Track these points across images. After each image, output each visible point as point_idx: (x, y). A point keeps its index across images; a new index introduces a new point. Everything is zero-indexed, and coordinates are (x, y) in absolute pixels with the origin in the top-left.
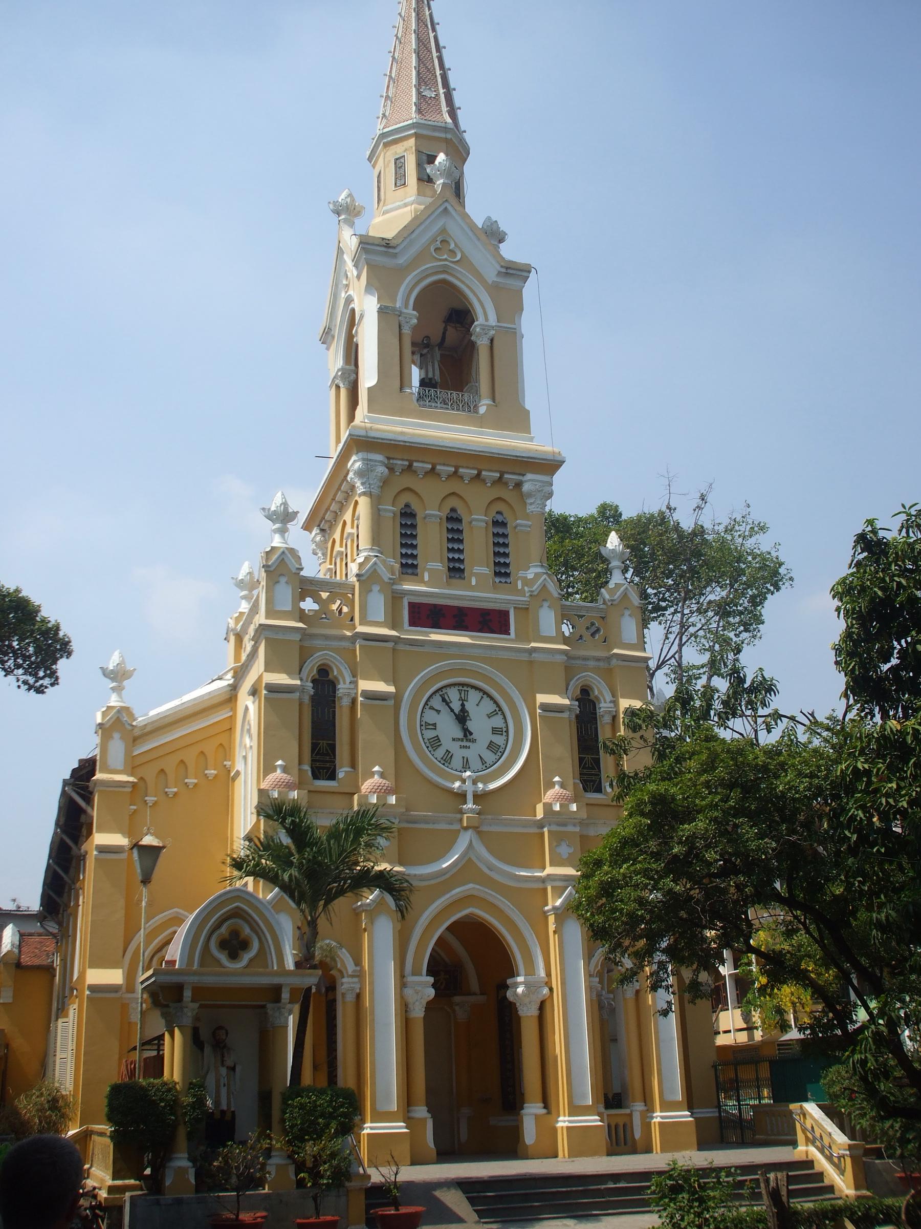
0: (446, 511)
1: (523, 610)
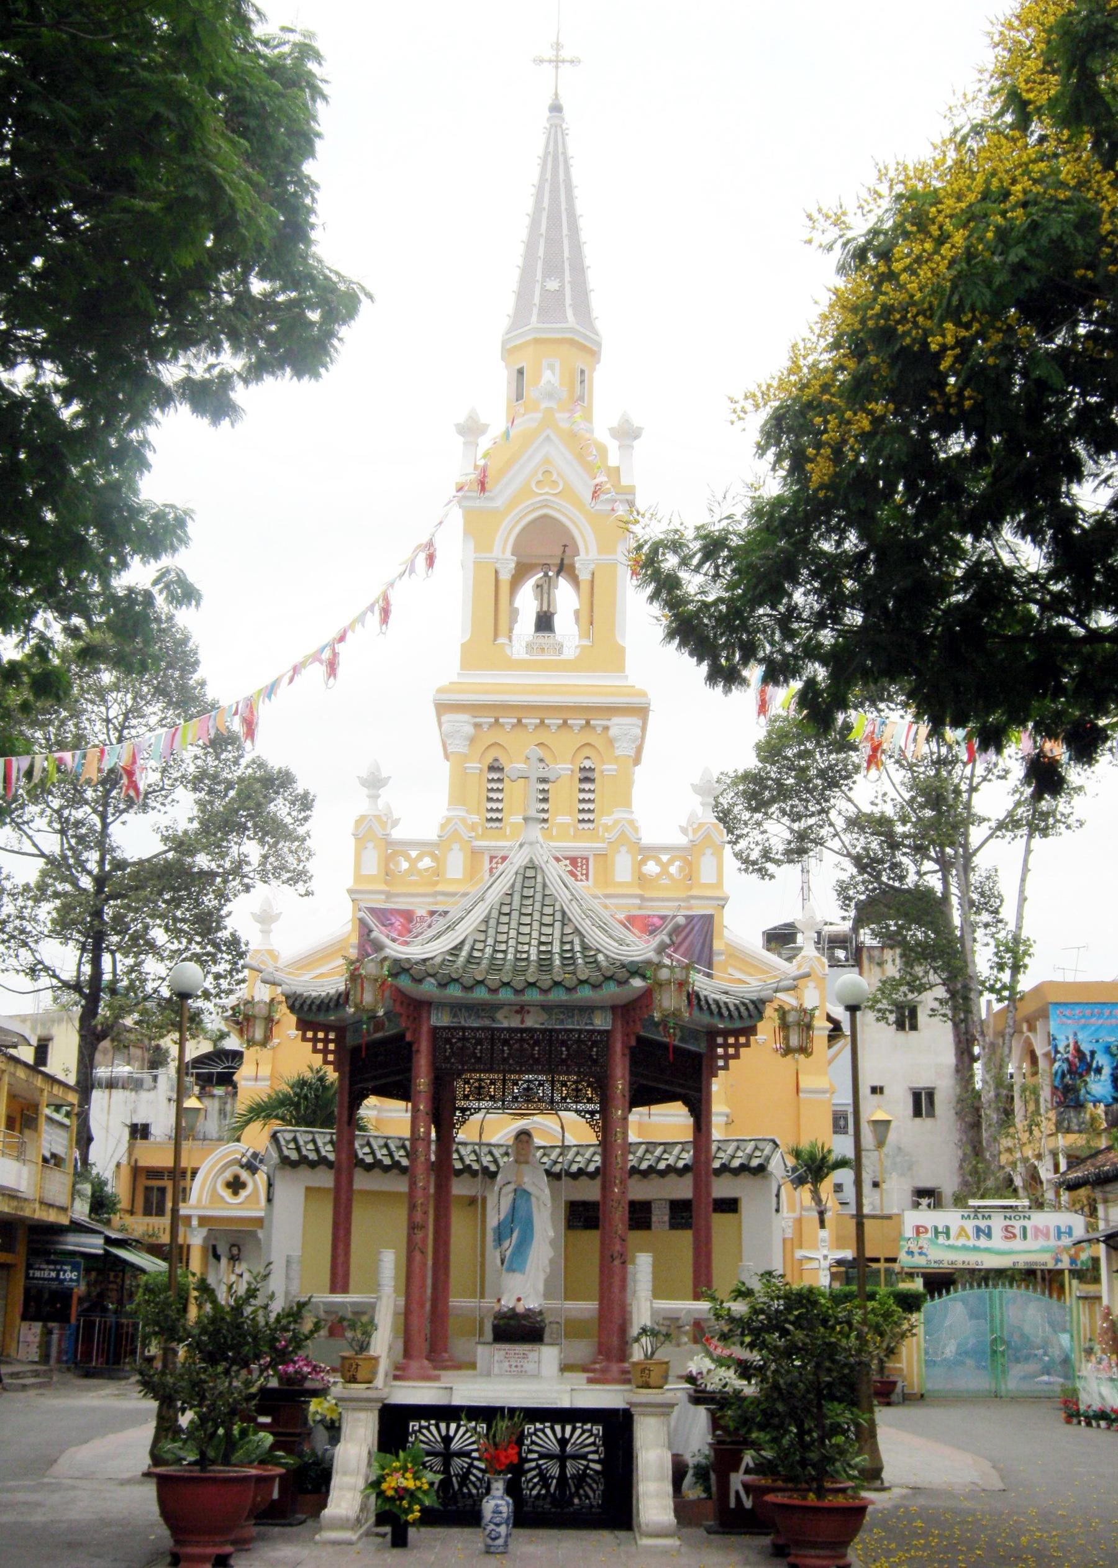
0: (489, 760)
1: (602, 856)
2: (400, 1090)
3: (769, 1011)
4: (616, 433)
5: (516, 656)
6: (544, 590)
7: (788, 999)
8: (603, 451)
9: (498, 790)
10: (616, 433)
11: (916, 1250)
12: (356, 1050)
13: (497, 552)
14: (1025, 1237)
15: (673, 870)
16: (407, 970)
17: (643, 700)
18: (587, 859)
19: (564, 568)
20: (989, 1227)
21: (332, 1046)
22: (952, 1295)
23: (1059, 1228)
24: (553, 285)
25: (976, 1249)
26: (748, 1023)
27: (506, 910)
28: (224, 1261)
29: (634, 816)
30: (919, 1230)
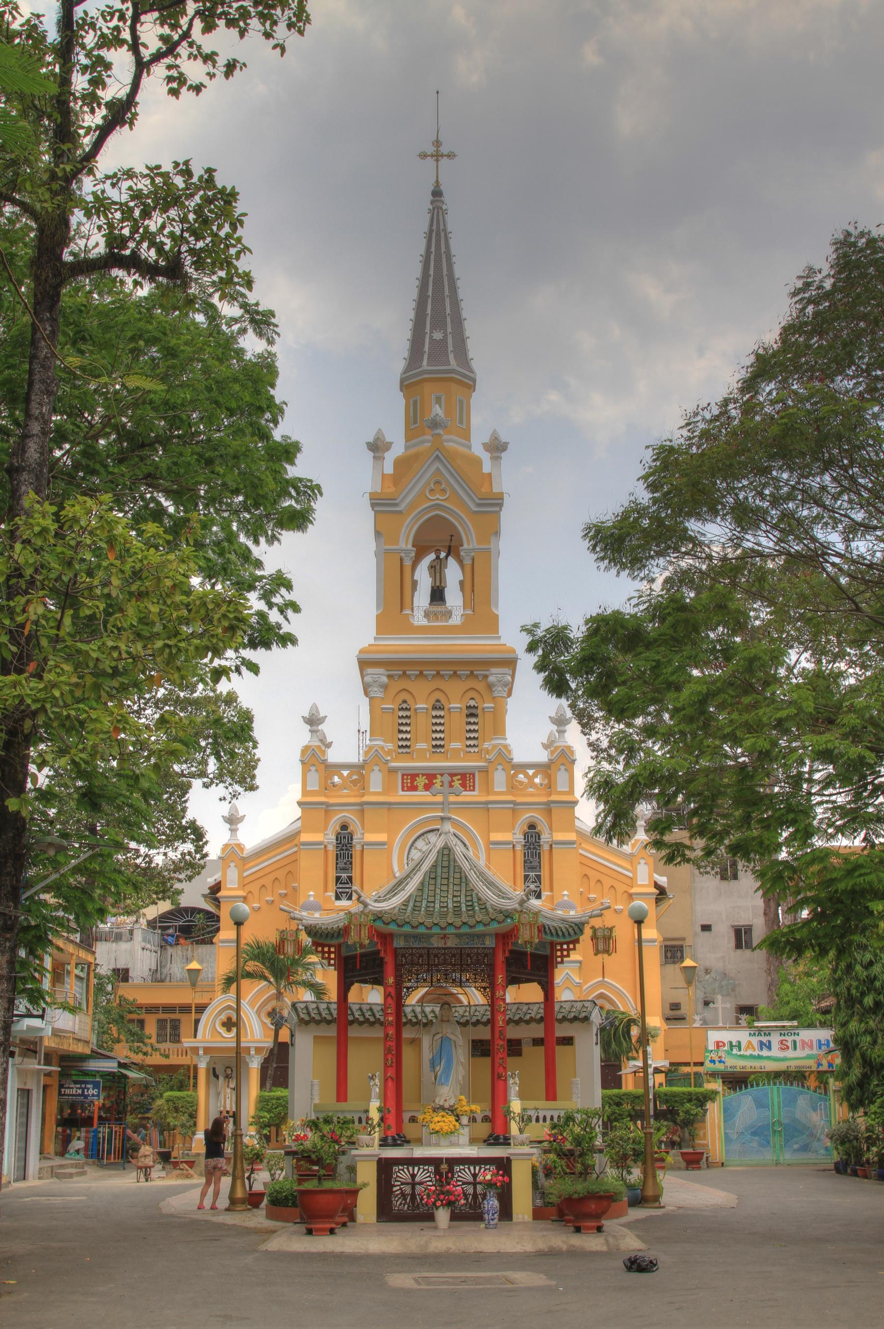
1: (485, 771)
2: (377, 981)
3: (588, 932)
4: (488, 447)
5: (416, 623)
6: (437, 569)
7: (597, 923)
8: (478, 462)
9: (406, 724)
10: (488, 447)
11: (717, 1059)
12: (347, 958)
13: (402, 545)
14: (795, 1048)
15: (537, 780)
16: (380, 918)
17: (512, 656)
18: (474, 775)
19: (453, 550)
20: (769, 1042)
21: (333, 956)
22: (744, 1091)
23: (820, 1041)
24: (438, 336)
25: (759, 1057)
26: (575, 938)
27: (433, 876)
28: (221, 1078)
29: (508, 742)
30: (718, 1044)
